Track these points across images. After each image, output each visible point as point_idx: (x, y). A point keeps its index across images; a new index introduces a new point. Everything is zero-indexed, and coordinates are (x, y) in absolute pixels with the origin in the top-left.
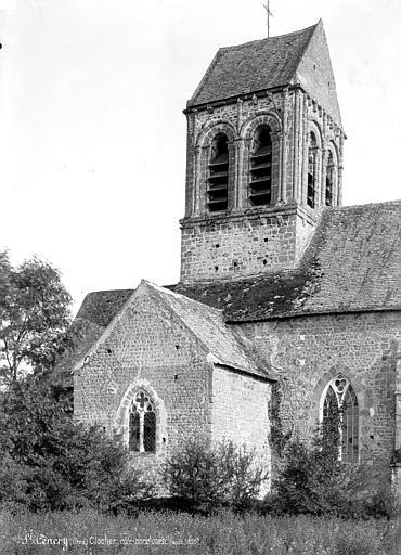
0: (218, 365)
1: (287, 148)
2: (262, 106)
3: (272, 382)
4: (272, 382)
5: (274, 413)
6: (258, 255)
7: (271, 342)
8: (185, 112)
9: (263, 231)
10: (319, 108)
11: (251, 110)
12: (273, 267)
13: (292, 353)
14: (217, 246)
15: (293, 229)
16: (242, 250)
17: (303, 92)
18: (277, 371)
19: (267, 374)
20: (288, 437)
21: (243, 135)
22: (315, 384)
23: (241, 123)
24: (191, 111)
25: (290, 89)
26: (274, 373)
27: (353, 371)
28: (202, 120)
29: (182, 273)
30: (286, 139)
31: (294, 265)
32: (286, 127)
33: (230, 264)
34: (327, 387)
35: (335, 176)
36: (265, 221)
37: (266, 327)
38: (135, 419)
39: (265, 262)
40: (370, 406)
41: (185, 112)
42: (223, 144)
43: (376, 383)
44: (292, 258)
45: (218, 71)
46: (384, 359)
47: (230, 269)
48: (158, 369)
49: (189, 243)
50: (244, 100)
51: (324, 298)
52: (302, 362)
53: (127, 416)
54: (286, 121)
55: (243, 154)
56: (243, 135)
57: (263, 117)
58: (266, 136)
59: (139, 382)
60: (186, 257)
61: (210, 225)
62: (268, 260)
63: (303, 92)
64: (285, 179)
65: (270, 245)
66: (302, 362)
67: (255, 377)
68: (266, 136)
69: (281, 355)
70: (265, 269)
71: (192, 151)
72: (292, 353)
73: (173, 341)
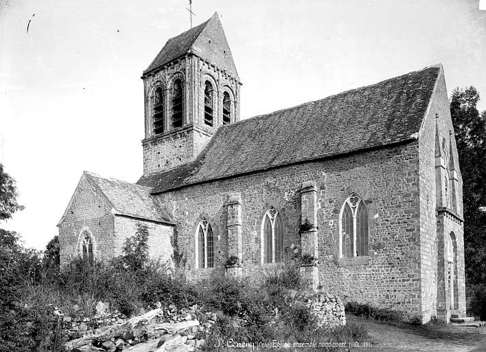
0: (116, 215)
1: (188, 91)
2: (177, 68)
3: (173, 225)
4: (173, 225)
5: (175, 243)
6: (177, 156)
7: (173, 204)
8: (142, 78)
9: (179, 142)
10: (213, 66)
11: (171, 71)
12: (184, 162)
13: (182, 208)
14: (159, 153)
15: (192, 138)
16: (170, 154)
17: (196, 56)
18: (176, 219)
19: (169, 221)
20: (181, 256)
21: (169, 87)
22: (193, 225)
23: (167, 80)
24: (146, 76)
25: (189, 56)
26: (173, 221)
27: (210, 215)
28: (150, 81)
29: (144, 170)
30: (187, 86)
31: (193, 160)
32: (187, 78)
33: (165, 163)
34: (199, 226)
35: (232, 107)
36: (179, 136)
37: (170, 195)
38: (84, 247)
39: (180, 159)
40: (218, 234)
41: (142, 78)
42: (160, 91)
43: (221, 221)
44: (192, 156)
45: (168, 48)
46: (224, 206)
47: (165, 165)
48: (92, 220)
49: (146, 153)
50: (168, 66)
51: (203, 173)
52: (187, 213)
53: (81, 248)
54: (187, 75)
55: (169, 97)
56: (169, 87)
57: (177, 75)
58: (179, 83)
59: (86, 228)
60: (146, 160)
61: (155, 141)
62: (182, 158)
63: (196, 56)
64: (187, 109)
65: (182, 149)
66: (187, 213)
67: (163, 224)
68: (179, 83)
69: (177, 210)
70: (180, 163)
71: (146, 101)
72: (182, 208)
73: (97, 203)
